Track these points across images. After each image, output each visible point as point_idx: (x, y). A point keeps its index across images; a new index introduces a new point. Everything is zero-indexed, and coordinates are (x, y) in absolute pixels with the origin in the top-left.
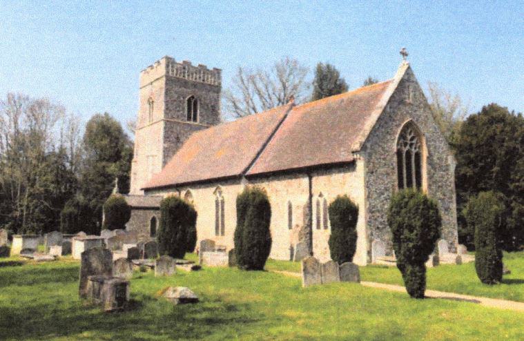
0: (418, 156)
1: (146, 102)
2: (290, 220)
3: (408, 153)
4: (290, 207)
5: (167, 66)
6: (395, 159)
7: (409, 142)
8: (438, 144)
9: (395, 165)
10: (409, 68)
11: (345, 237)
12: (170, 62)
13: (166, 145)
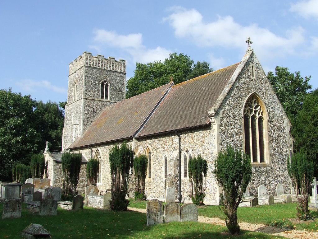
0: (261, 119)
2: (166, 171)
4: (166, 161)
6: (243, 121)
8: (276, 111)
9: (243, 127)
10: (253, 53)
13: (85, 117)
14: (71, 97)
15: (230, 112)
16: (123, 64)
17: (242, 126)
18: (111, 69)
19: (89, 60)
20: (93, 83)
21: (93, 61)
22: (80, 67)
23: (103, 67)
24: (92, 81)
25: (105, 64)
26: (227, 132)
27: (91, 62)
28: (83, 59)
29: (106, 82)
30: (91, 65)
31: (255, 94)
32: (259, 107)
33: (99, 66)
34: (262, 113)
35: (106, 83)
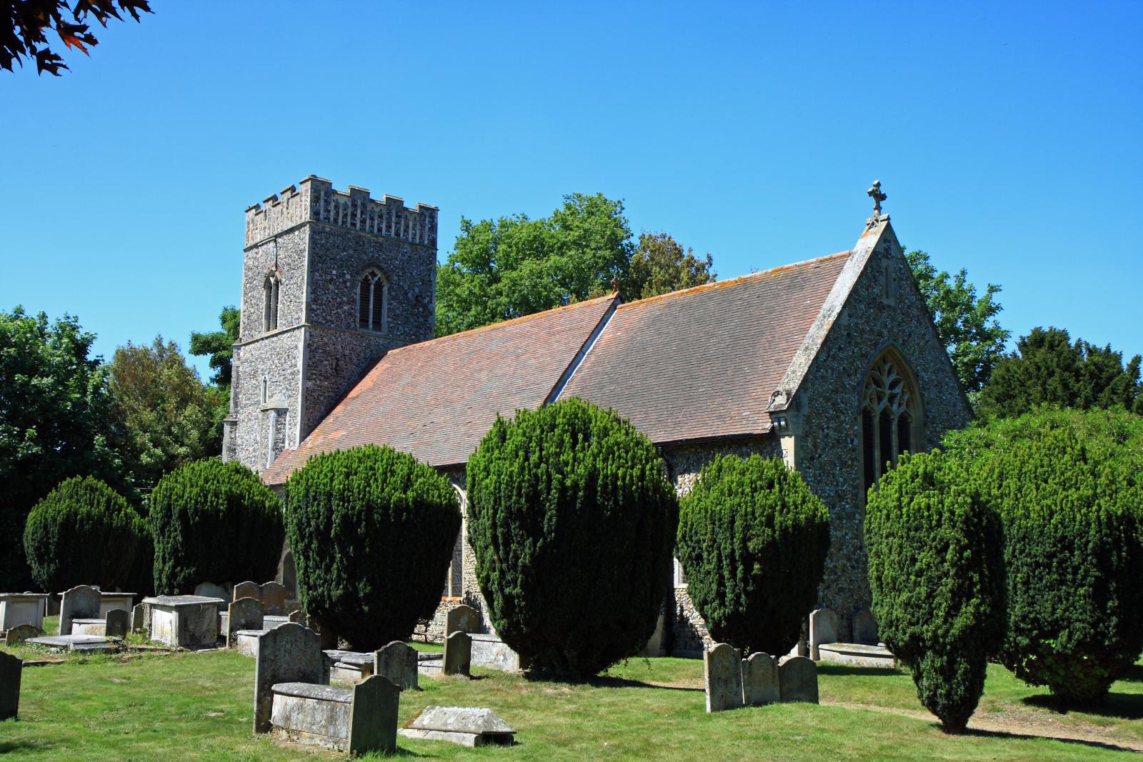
1: (259, 282)
3: (885, 416)
5: (315, 200)
7: (888, 392)
11: (508, 261)
12: (321, 191)
14: (254, 317)
15: (827, 399)
16: (427, 219)
17: (856, 442)
19: (322, 203)
20: (335, 277)
21: (336, 207)
22: (291, 225)
24: (334, 272)
25: (372, 219)
26: (820, 456)
28: (303, 198)
31: (891, 347)
35: (376, 279)
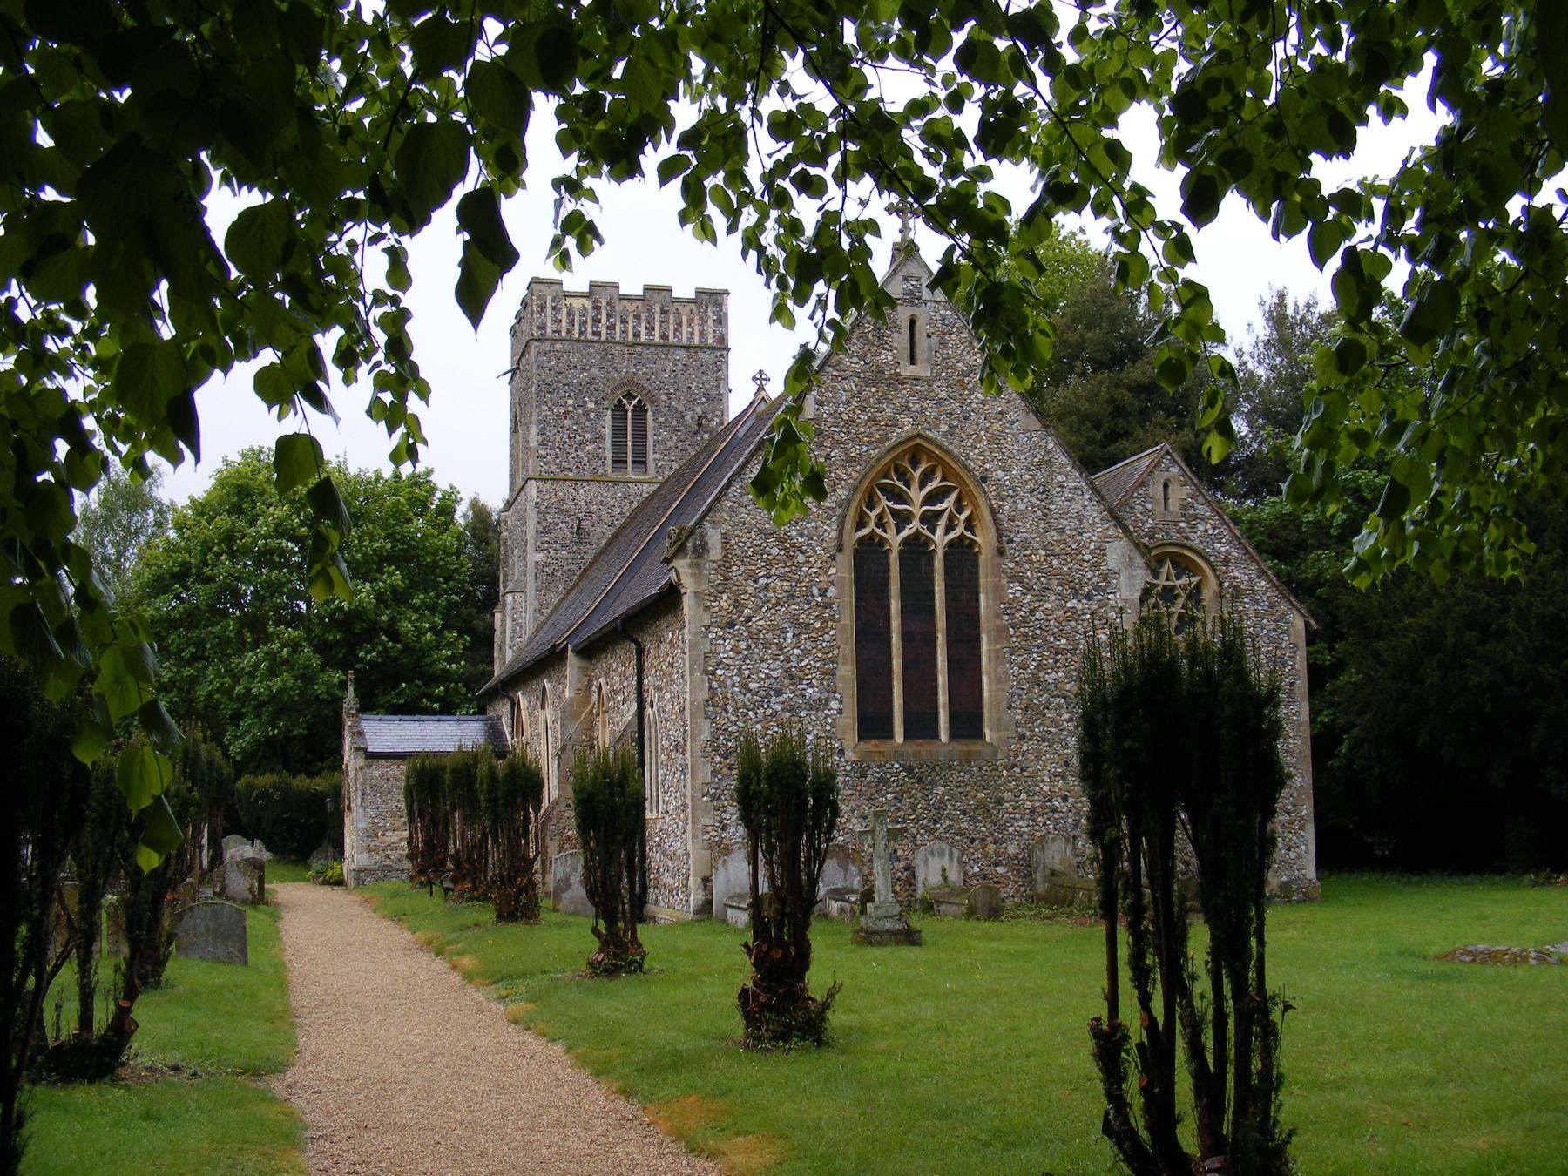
18: (657, 339)
19: (549, 311)
20: (571, 409)
21: (568, 314)
23: (618, 335)
25: (624, 322)
26: (749, 619)
27: (560, 321)
29: (635, 397)
30: (559, 332)
31: (919, 441)
32: (953, 496)
33: (598, 334)
34: (969, 520)
35: (634, 402)
